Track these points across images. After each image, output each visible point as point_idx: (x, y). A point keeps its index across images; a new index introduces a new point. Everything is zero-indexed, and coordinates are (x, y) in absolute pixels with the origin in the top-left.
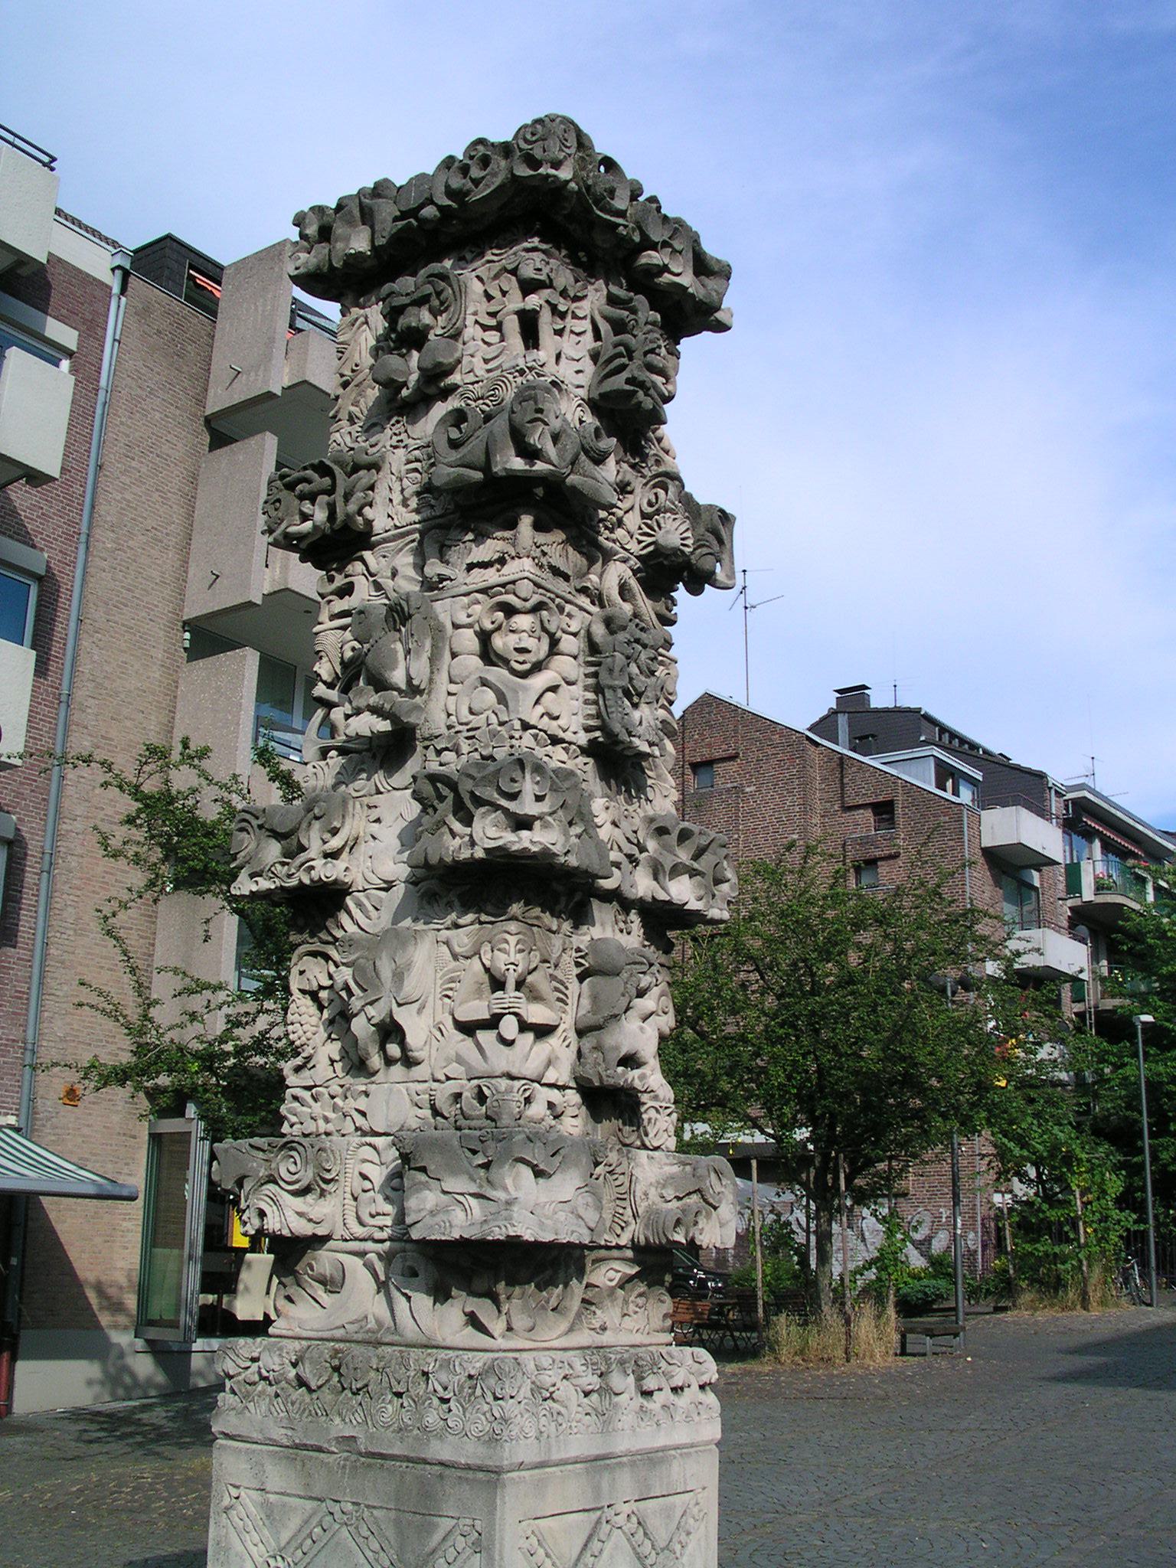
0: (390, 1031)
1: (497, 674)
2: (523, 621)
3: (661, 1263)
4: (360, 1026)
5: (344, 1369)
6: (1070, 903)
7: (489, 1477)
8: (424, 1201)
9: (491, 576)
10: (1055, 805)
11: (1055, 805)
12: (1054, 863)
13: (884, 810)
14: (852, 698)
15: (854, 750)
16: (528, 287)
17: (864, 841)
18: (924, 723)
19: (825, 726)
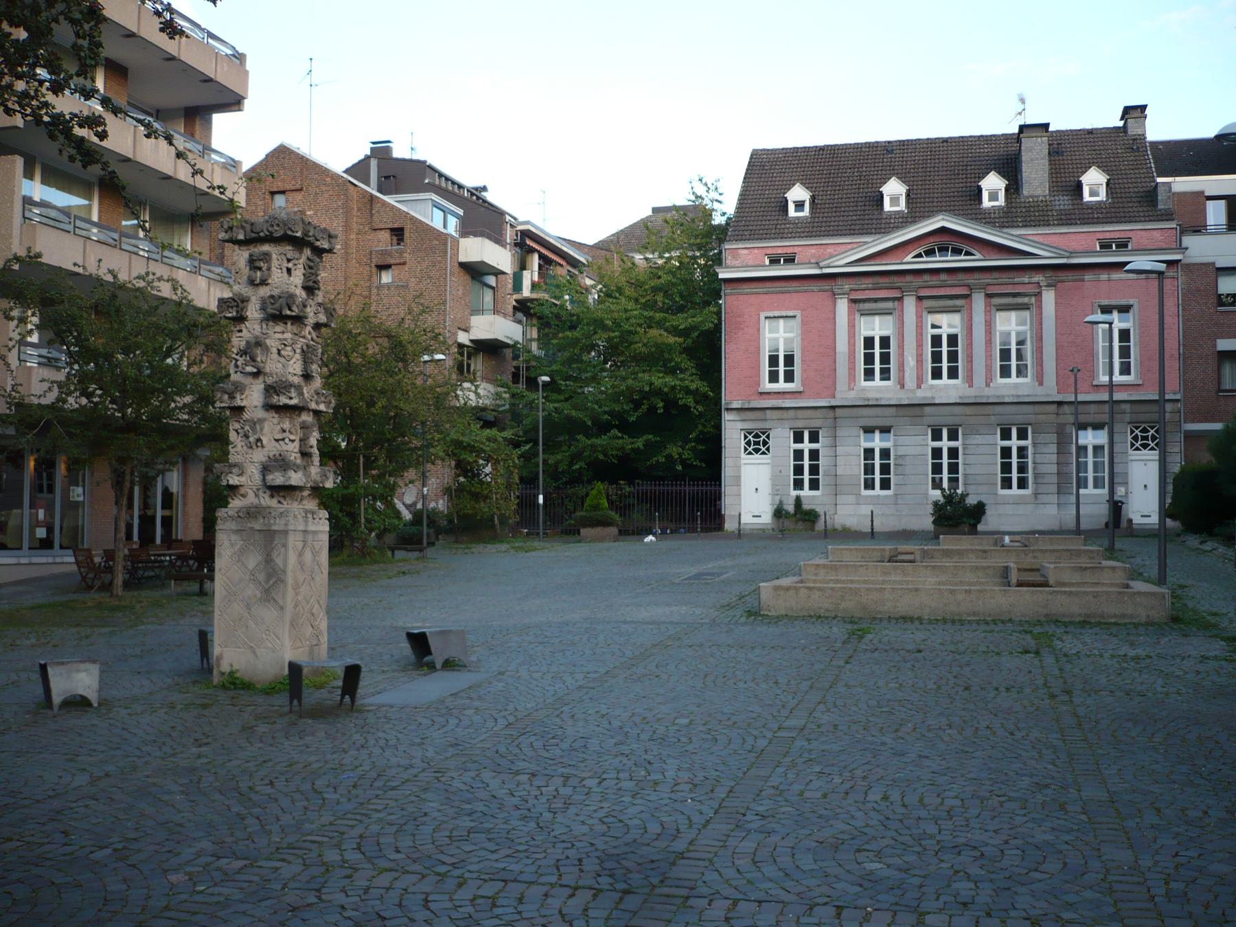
0: (259, 440)
1: (282, 360)
2: (289, 348)
3: (317, 491)
4: (251, 439)
5: (252, 513)
6: (515, 297)
7: (286, 532)
8: (269, 477)
9: (280, 336)
10: (509, 235)
11: (509, 235)
12: (503, 273)
13: (398, 233)
14: (381, 152)
15: (380, 191)
16: (289, 260)
17: (384, 253)
18: (428, 170)
19: (358, 170)
